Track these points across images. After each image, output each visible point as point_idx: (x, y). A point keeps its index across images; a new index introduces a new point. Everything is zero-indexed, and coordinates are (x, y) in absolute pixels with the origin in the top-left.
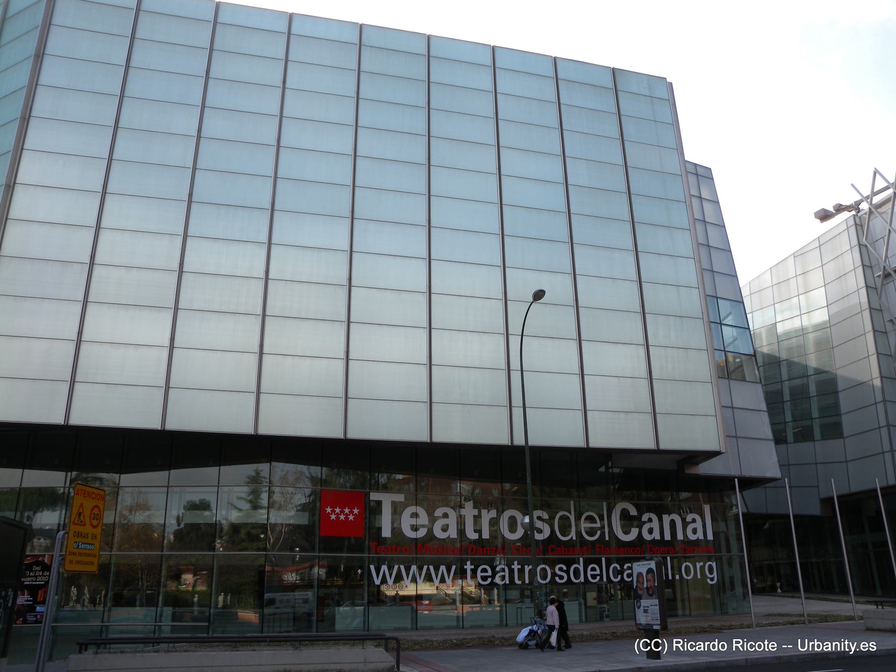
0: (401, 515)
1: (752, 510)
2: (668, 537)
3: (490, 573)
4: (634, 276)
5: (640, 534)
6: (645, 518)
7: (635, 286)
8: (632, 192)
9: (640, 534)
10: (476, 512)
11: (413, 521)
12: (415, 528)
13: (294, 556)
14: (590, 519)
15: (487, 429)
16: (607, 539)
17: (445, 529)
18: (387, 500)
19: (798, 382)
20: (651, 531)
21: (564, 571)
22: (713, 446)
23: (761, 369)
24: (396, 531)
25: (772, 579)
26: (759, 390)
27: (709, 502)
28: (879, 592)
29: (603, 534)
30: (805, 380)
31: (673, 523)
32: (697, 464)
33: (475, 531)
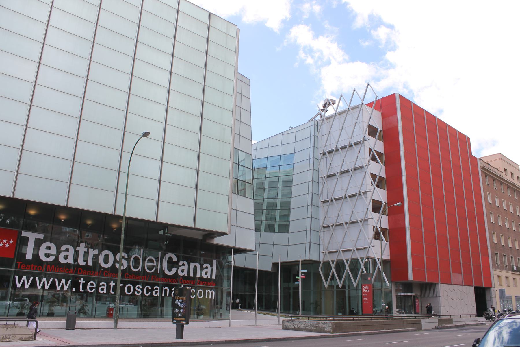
0: (37, 247)
1: (237, 265)
2: (191, 275)
3: (94, 286)
4: (198, 131)
5: (177, 271)
6: (181, 263)
7: (198, 137)
8: (206, 84)
9: (177, 271)
10: (86, 250)
11: (47, 251)
12: (47, 255)
13: (298, 276)
14: (151, 261)
15: (101, 203)
16: (159, 272)
17: (66, 257)
18: (32, 237)
19: (272, 200)
20: (183, 271)
21: (140, 289)
22: (223, 230)
23: (255, 190)
24: (36, 256)
25: (244, 303)
26: (252, 202)
27: (216, 259)
28: (291, 311)
29: (157, 270)
30: (275, 200)
31: (195, 267)
32: (214, 238)
33: (84, 261)
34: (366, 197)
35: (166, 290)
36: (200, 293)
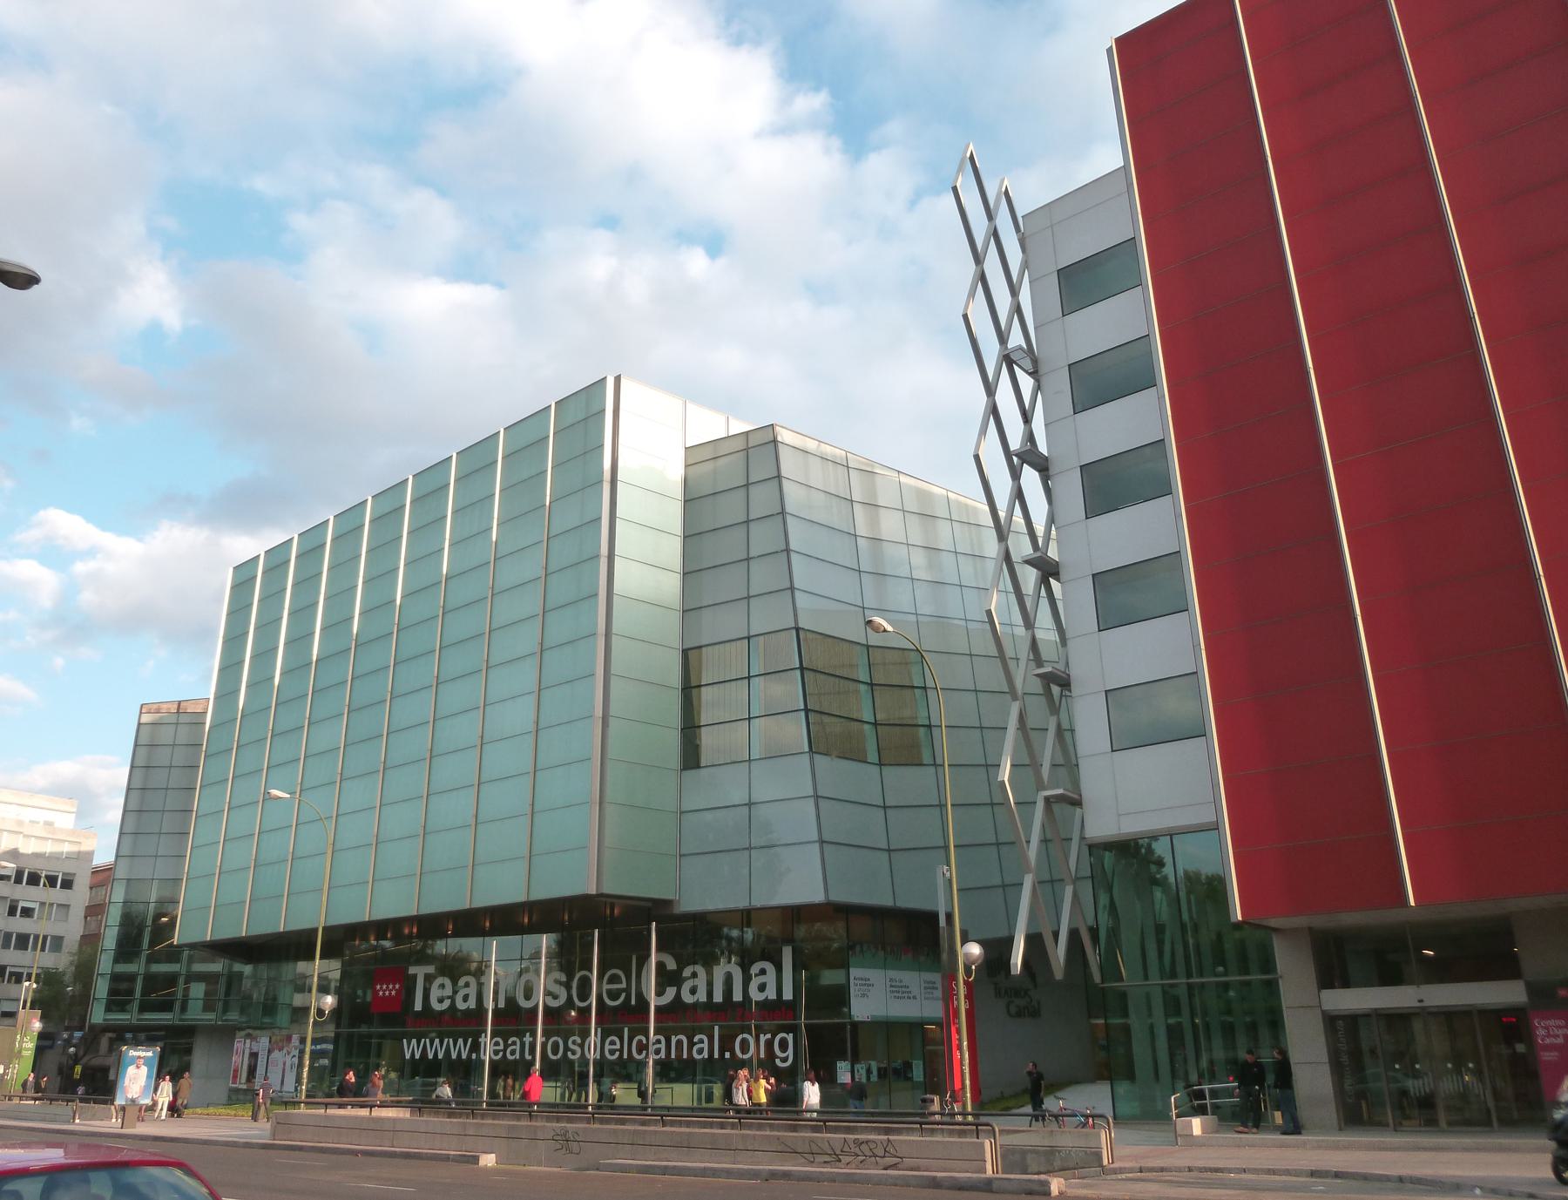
6: (687, 972)
29: (628, 998)
34: (91, 553)
35: (679, 1043)
36: (555, 1052)
